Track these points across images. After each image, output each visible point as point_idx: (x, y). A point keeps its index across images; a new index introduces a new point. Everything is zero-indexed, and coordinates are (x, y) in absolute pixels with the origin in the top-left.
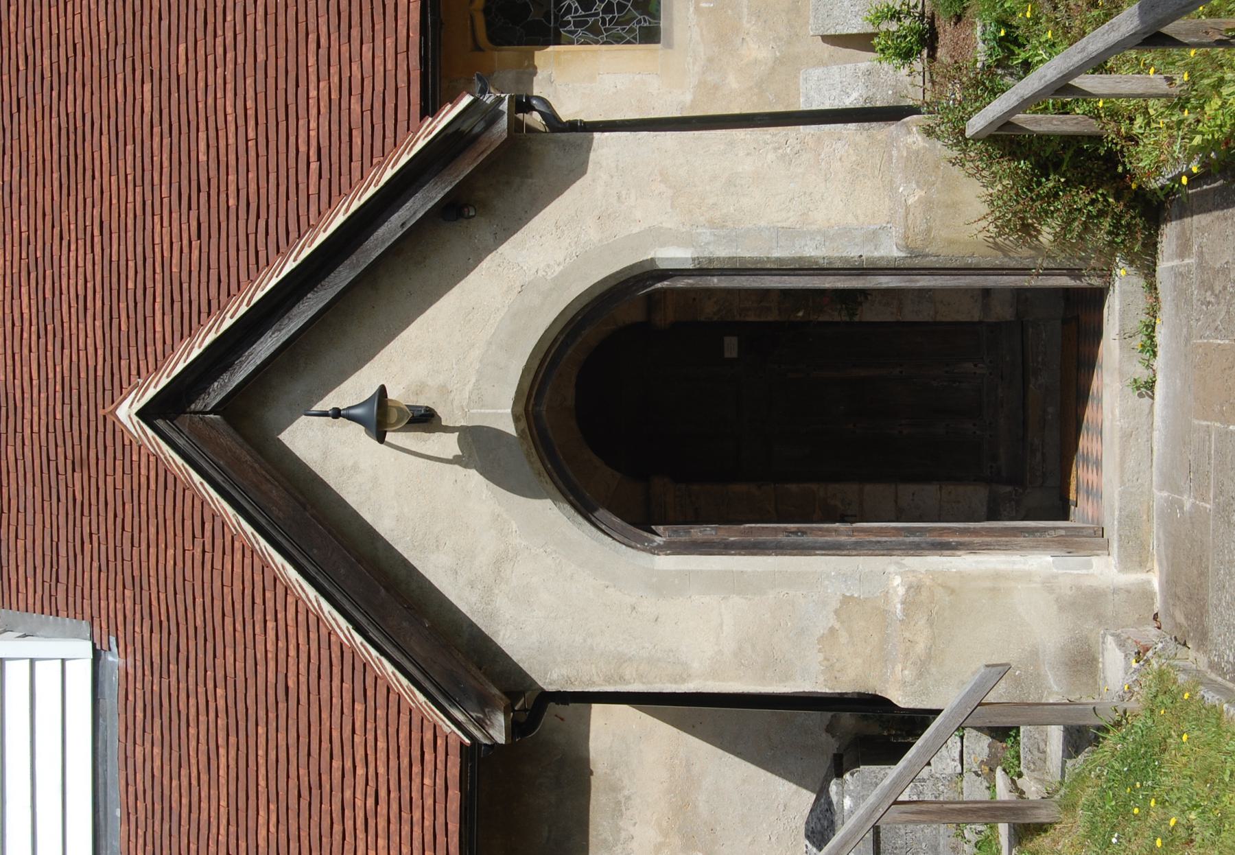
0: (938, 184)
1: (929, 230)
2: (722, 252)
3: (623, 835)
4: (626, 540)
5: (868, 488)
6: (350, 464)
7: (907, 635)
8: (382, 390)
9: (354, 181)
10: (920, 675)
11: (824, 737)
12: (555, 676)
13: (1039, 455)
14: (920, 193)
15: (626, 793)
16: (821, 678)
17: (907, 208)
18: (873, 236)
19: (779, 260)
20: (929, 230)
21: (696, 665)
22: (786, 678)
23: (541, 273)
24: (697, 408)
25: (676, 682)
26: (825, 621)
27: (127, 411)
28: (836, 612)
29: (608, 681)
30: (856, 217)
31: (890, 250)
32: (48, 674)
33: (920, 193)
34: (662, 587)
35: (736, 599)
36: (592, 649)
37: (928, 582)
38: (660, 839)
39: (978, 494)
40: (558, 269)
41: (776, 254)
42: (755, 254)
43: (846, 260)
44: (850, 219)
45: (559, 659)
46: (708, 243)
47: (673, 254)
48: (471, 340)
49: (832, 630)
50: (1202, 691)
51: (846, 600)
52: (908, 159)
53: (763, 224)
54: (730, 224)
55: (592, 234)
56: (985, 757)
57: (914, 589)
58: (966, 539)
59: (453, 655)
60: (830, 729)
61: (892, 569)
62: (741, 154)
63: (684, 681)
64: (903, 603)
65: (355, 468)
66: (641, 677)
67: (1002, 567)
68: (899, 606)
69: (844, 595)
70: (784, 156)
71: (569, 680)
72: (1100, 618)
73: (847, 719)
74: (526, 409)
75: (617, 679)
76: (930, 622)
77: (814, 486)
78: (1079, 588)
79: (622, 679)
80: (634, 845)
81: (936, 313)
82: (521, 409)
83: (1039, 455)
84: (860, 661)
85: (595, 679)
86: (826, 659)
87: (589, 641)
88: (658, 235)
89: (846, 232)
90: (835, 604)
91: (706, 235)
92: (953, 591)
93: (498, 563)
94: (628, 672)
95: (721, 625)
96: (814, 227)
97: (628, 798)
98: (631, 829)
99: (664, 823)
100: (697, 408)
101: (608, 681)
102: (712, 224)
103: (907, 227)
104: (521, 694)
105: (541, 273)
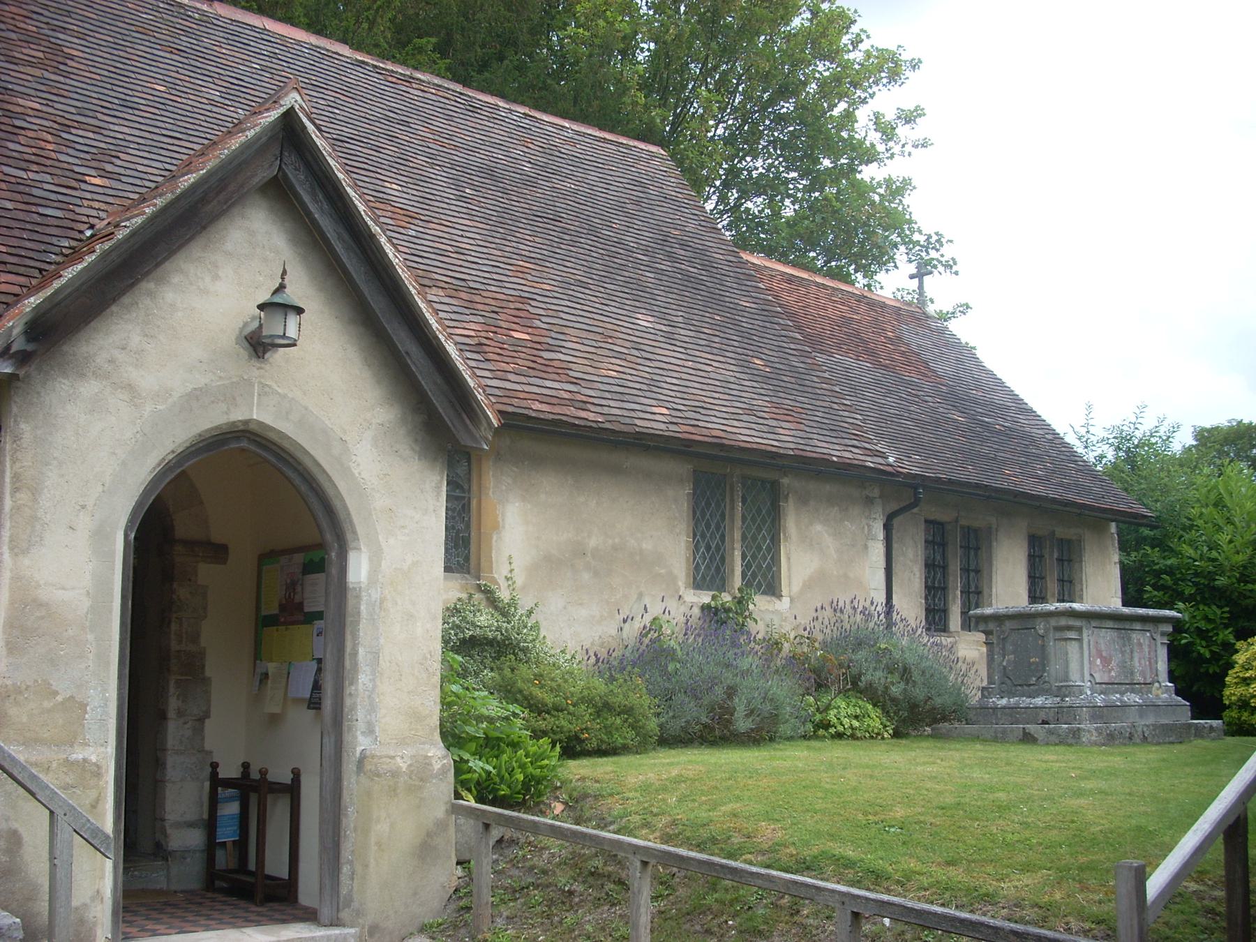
0: (411, 782)
1: (378, 775)
6: (220, 274)
7: (54, 765)
9: (469, 362)
12: (23, 426)
14: (404, 767)
17: (393, 758)
18: (370, 731)
20: (378, 775)
21: (27, 562)
26: (64, 688)
27: (292, 99)
28: (72, 697)
33: (404, 767)
34: (100, 535)
35: (86, 603)
40: (356, 472)
41: (361, 651)
45: (39, 432)
46: (370, 596)
47: (359, 569)
48: (330, 401)
49: (56, 693)
50: (1142, 529)
51: (83, 706)
53: (382, 641)
54: (383, 614)
55: (380, 502)
56: (270, 778)
63: (11, 549)
64: (85, 760)
65: (216, 277)
68: (81, 756)
69: (87, 705)
70: (426, 658)
75: (17, 485)
78: (95, 924)
79: (16, 490)
84: (25, 720)
85: (18, 465)
88: (376, 557)
89: (373, 708)
91: (375, 595)
93: (130, 387)
95: (64, 589)
96: (378, 683)
102: (382, 601)
103: (381, 757)
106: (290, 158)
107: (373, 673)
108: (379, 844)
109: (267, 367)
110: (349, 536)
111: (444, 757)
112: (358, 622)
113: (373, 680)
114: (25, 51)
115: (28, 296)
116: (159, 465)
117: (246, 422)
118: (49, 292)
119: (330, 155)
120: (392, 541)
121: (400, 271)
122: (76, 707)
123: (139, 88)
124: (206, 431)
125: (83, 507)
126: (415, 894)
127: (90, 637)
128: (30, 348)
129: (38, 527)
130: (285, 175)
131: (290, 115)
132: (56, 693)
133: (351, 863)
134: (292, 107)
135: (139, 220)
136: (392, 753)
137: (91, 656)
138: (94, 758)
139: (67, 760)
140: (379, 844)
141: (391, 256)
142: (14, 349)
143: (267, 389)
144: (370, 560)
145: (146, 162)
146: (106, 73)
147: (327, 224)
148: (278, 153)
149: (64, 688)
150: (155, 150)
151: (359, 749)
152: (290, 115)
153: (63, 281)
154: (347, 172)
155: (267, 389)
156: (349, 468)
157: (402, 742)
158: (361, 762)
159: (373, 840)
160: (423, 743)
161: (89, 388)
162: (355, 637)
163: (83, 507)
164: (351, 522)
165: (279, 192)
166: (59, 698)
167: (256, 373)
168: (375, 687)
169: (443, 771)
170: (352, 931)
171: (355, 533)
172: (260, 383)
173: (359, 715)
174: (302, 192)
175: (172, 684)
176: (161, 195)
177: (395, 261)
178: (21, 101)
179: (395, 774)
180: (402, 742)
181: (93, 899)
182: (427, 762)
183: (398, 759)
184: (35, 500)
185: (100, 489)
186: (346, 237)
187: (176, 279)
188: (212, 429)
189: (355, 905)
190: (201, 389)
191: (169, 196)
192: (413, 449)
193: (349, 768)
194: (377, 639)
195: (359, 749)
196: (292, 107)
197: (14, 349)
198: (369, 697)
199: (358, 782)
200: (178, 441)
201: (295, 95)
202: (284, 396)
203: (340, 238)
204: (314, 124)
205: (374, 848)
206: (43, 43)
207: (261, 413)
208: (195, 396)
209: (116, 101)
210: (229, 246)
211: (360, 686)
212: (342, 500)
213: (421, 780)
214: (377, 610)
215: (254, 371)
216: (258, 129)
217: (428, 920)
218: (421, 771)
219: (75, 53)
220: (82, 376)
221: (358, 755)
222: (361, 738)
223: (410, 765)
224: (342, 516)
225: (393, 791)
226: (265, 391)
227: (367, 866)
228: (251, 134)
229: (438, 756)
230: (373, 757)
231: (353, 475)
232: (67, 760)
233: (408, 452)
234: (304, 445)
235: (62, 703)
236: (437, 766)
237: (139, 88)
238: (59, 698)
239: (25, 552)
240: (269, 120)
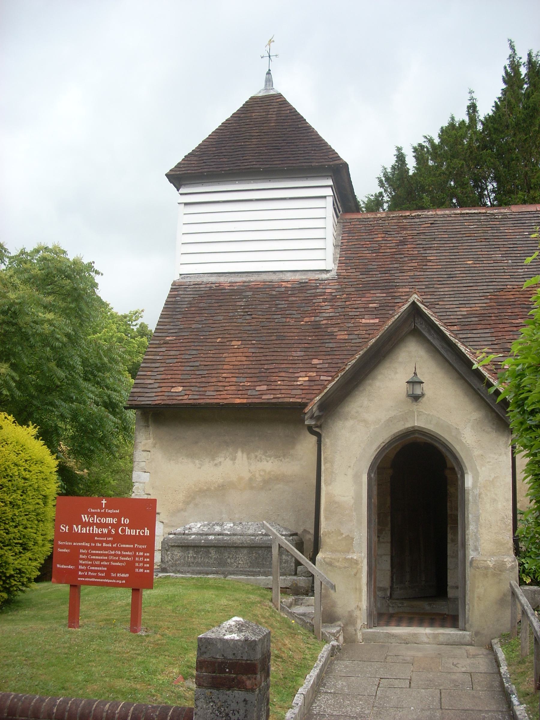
1: (478, 568)
2: (470, 497)
3: (269, 459)
4: (246, 284)
5: (389, 545)
6: (398, 371)
7: (341, 560)
8: (423, 383)
10: (327, 563)
11: (302, 529)
12: (326, 440)
13: (400, 605)
15: (283, 460)
16: (326, 530)
17: (486, 561)
18: (476, 549)
19: (468, 517)
20: (478, 568)
21: (330, 488)
22: (326, 518)
23: (463, 435)
24: (417, 490)
25: (325, 481)
26: (345, 531)
27: (415, 297)
28: (348, 536)
29: (325, 458)
30: (483, 543)
31: (471, 554)
32: (319, 254)
34: (357, 477)
35: (352, 501)
36: (336, 452)
37: (359, 567)
38: (267, 471)
39: (385, 582)
40: (464, 441)
42: (470, 509)
43: (468, 540)
44: (482, 541)
47: (469, 481)
48: (450, 415)
49: (342, 534)
51: (352, 539)
52: (503, 561)
53: (481, 511)
54: (480, 500)
55: (477, 452)
57: (356, 562)
58: (373, 580)
59: (333, 405)
60: (305, 531)
61: (363, 555)
62: (504, 504)
63: (325, 484)
65: (396, 373)
66: (326, 469)
67: (363, 591)
70: (504, 518)
71: (325, 445)
72: (346, 625)
73: (310, 537)
74: (417, 430)
76: (345, 568)
77: (389, 526)
78: (356, 618)
79: (325, 463)
80: (265, 463)
81: (451, 569)
82: (416, 429)
83: (400, 605)
84: (332, 543)
86: (332, 532)
87: (338, 452)
88: (476, 476)
89: (477, 540)
90: (351, 536)
91: (476, 492)
92: (355, 575)
93: (364, 421)
94: (328, 465)
95: (344, 496)
96: (480, 529)
97: (281, 461)
98: (271, 461)
99: (272, 473)
100: (417, 490)
101: (325, 458)
103: (479, 561)
104: (321, 430)
105: (463, 435)
106: (418, 320)
107: (477, 525)
108: (479, 598)
109: (420, 404)
110: (464, 468)
111: (512, 562)
112: (468, 504)
113: (477, 528)
114: (409, 265)
115: (316, 397)
116: (378, 448)
117: (413, 427)
118: (323, 394)
119: (432, 315)
120: (483, 469)
121: (468, 356)
122: (350, 539)
123: (459, 266)
124: (396, 433)
125: (350, 467)
126: (498, 620)
127: (354, 514)
128: (320, 414)
129: (334, 475)
130: (417, 327)
131: (414, 303)
132: (342, 534)
133: (468, 604)
134: (414, 301)
135: (354, 361)
136: (485, 559)
137: (355, 520)
138: (355, 558)
139: (345, 558)
140: (479, 598)
141: (463, 350)
142: (315, 415)
143: (420, 413)
144: (473, 477)
145: (451, 303)
146: (445, 263)
147: (436, 343)
148: (412, 320)
149: (345, 533)
150: (457, 295)
151: (471, 557)
152: (414, 303)
153: (328, 389)
154: (440, 320)
155: (420, 413)
156: (461, 440)
157: (493, 554)
158: (471, 562)
159: (476, 595)
160: (504, 555)
161: (349, 423)
162: (468, 510)
163: (350, 467)
164: (463, 462)
165: (416, 333)
166: (344, 536)
167: (415, 407)
168: (478, 531)
169: (513, 568)
170: (468, 633)
171: (465, 467)
172: (417, 411)
173: (470, 543)
174: (424, 333)
175: (448, 528)
176: (362, 350)
177: (465, 352)
178: (401, 290)
179: (487, 568)
180: (493, 554)
181: (355, 609)
182: (503, 563)
183: (488, 562)
184: (332, 466)
185: (356, 459)
186: (445, 346)
187: (380, 377)
188: (399, 432)
189: (470, 622)
190: (392, 417)
191: (365, 349)
192: (492, 428)
193: (468, 564)
194: (478, 511)
195: (471, 557)
196: (414, 301)
197: (315, 415)
198: (475, 535)
199: (470, 571)
200: (385, 438)
201: (416, 296)
202: (429, 415)
203: (443, 347)
204: (424, 305)
205: (476, 599)
206: (419, 258)
207: (419, 423)
208: (390, 420)
209: (446, 276)
210: (400, 359)
211: (471, 531)
212: (459, 453)
213: (500, 571)
214: (477, 498)
215: (415, 407)
216: (399, 314)
217: (504, 633)
218: (500, 568)
219: (432, 258)
220: (347, 419)
221: (470, 559)
222: (471, 552)
223: (494, 565)
224: (460, 460)
225: (486, 575)
226: (420, 414)
227: (474, 606)
228: (396, 317)
229: (510, 560)
230: (476, 560)
231: (463, 442)
232: (345, 558)
233: (490, 430)
234: (439, 433)
235: (345, 538)
236: (509, 565)
237: (459, 266)
238: (344, 536)
239: (330, 484)
240: (404, 309)
